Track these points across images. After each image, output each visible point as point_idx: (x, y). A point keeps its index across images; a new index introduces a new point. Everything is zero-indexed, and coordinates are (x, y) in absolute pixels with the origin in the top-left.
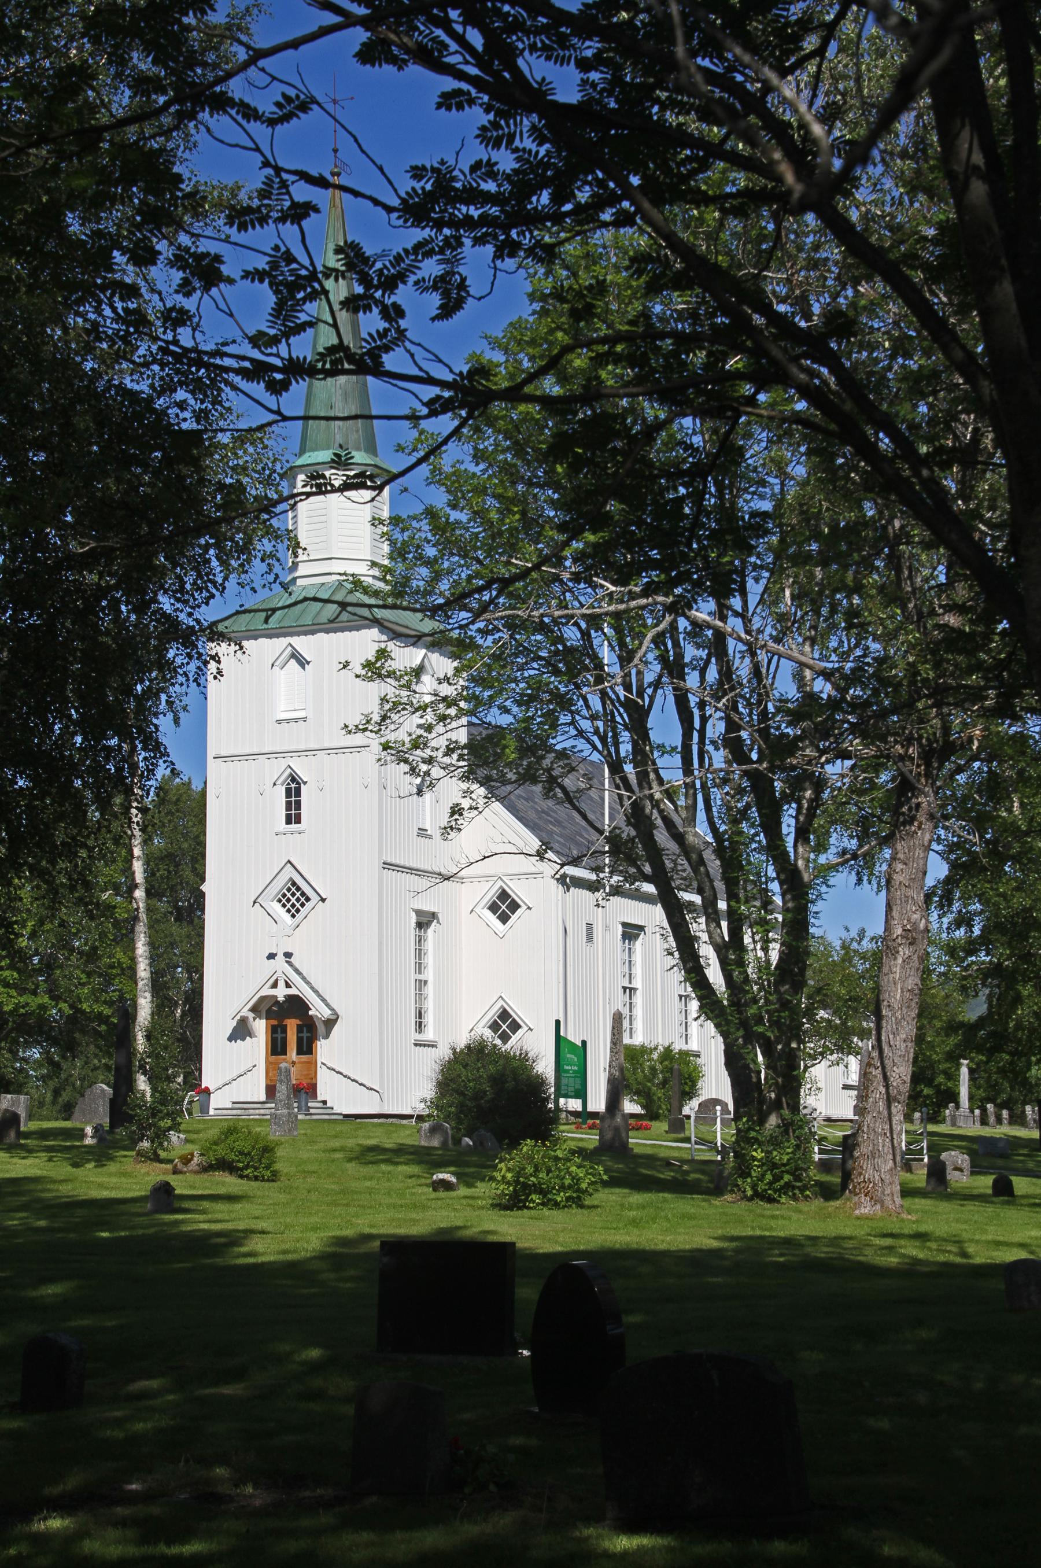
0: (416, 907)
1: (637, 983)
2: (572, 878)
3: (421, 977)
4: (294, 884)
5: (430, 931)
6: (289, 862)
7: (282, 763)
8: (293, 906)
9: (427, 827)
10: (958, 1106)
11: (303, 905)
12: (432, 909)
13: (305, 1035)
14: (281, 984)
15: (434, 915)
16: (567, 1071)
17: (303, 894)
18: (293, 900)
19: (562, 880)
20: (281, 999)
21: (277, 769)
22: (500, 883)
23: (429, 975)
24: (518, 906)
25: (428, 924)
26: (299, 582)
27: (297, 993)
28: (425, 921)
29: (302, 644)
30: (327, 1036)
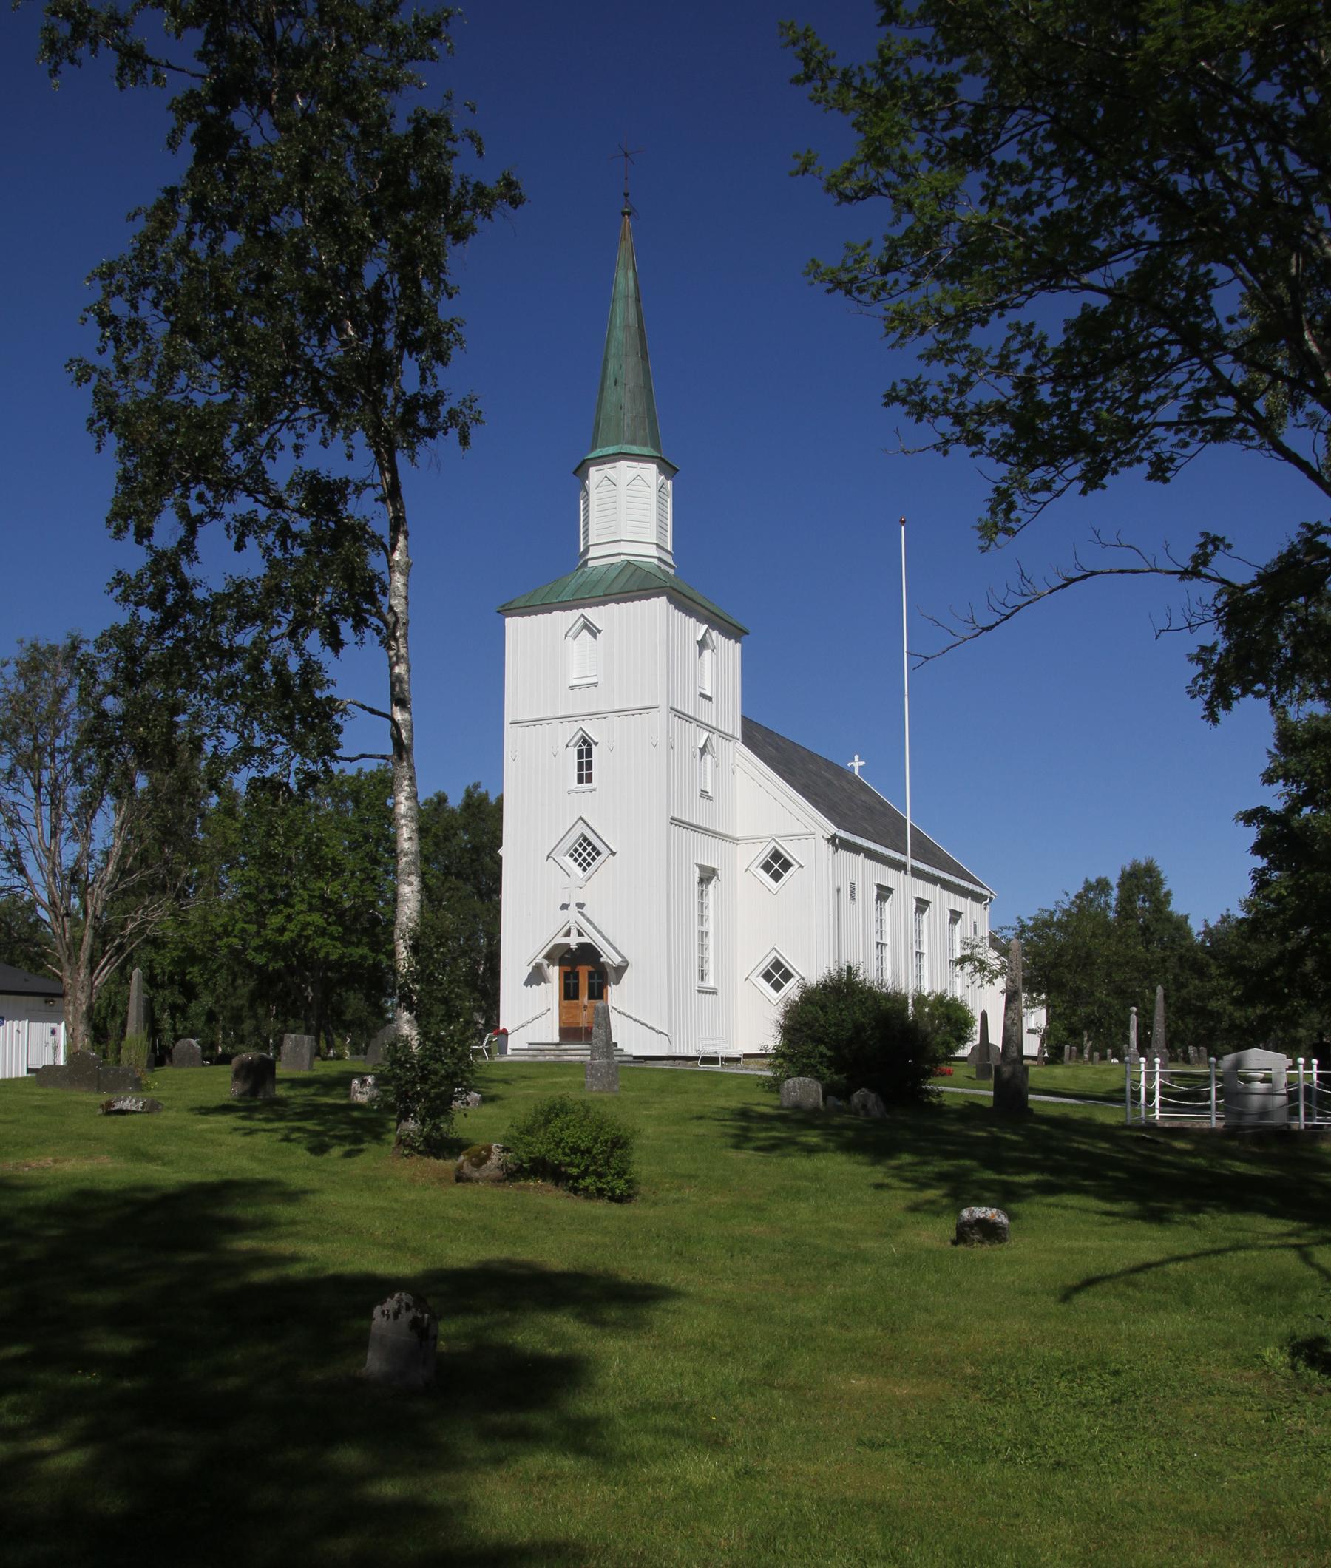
2: (841, 839)
5: (711, 886)
7: (576, 726)
8: (585, 860)
11: (594, 859)
13: (596, 981)
14: (574, 932)
17: (594, 849)
18: (585, 854)
20: (573, 946)
21: (569, 732)
22: (774, 844)
23: (710, 927)
26: (590, 564)
27: (589, 941)
29: (593, 614)
30: (617, 983)
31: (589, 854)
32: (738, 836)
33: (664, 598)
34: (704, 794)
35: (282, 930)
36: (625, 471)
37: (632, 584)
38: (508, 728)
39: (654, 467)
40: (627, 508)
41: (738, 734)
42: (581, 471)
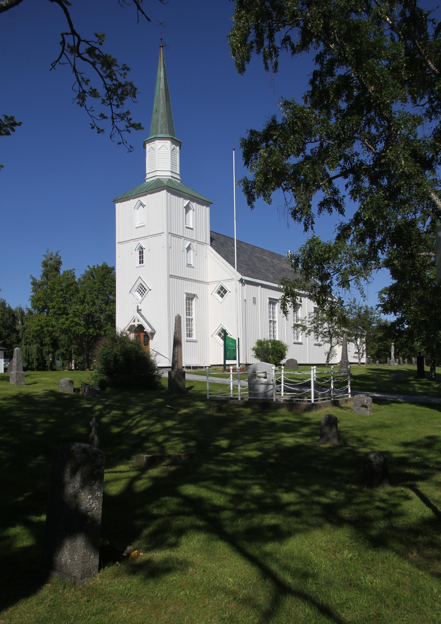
0: (186, 292)
1: (276, 319)
2: (245, 280)
3: (190, 317)
4: (142, 285)
5: (194, 301)
6: (140, 277)
7: (137, 242)
8: (142, 293)
9: (192, 264)
10: (390, 359)
11: (145, 292)
12: (194, 293)
14: (136, 320)
15: (195, 295)
16: (230, 350)
17: (145, 289)
18: (142, 291)
19: (241, 281)
20: (136, 326)
21: (135, 245)
22: (220, 284)
23: (194, 317)
24: (227, 291)
25: (192, 299)
26: (147, 181)
27: (141, 323)
28: (190, 298)
29: (143, 199)
30: (152, 339)
31: (143, 291)
32: (209, 281)
33: (165, 191)
34: (189, 265)
35: (63, 324)
36: (158, 144)
37: (158, 186)
38: (117, 245)
39: (169, 142)
40: (161, 158)
41: (208, 241)
42: (145, 147)
